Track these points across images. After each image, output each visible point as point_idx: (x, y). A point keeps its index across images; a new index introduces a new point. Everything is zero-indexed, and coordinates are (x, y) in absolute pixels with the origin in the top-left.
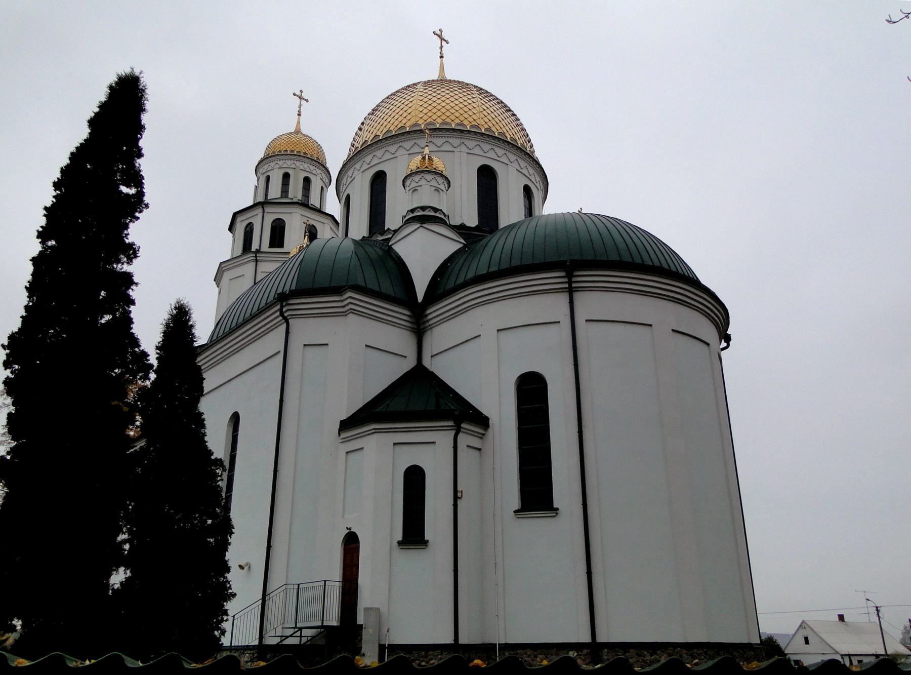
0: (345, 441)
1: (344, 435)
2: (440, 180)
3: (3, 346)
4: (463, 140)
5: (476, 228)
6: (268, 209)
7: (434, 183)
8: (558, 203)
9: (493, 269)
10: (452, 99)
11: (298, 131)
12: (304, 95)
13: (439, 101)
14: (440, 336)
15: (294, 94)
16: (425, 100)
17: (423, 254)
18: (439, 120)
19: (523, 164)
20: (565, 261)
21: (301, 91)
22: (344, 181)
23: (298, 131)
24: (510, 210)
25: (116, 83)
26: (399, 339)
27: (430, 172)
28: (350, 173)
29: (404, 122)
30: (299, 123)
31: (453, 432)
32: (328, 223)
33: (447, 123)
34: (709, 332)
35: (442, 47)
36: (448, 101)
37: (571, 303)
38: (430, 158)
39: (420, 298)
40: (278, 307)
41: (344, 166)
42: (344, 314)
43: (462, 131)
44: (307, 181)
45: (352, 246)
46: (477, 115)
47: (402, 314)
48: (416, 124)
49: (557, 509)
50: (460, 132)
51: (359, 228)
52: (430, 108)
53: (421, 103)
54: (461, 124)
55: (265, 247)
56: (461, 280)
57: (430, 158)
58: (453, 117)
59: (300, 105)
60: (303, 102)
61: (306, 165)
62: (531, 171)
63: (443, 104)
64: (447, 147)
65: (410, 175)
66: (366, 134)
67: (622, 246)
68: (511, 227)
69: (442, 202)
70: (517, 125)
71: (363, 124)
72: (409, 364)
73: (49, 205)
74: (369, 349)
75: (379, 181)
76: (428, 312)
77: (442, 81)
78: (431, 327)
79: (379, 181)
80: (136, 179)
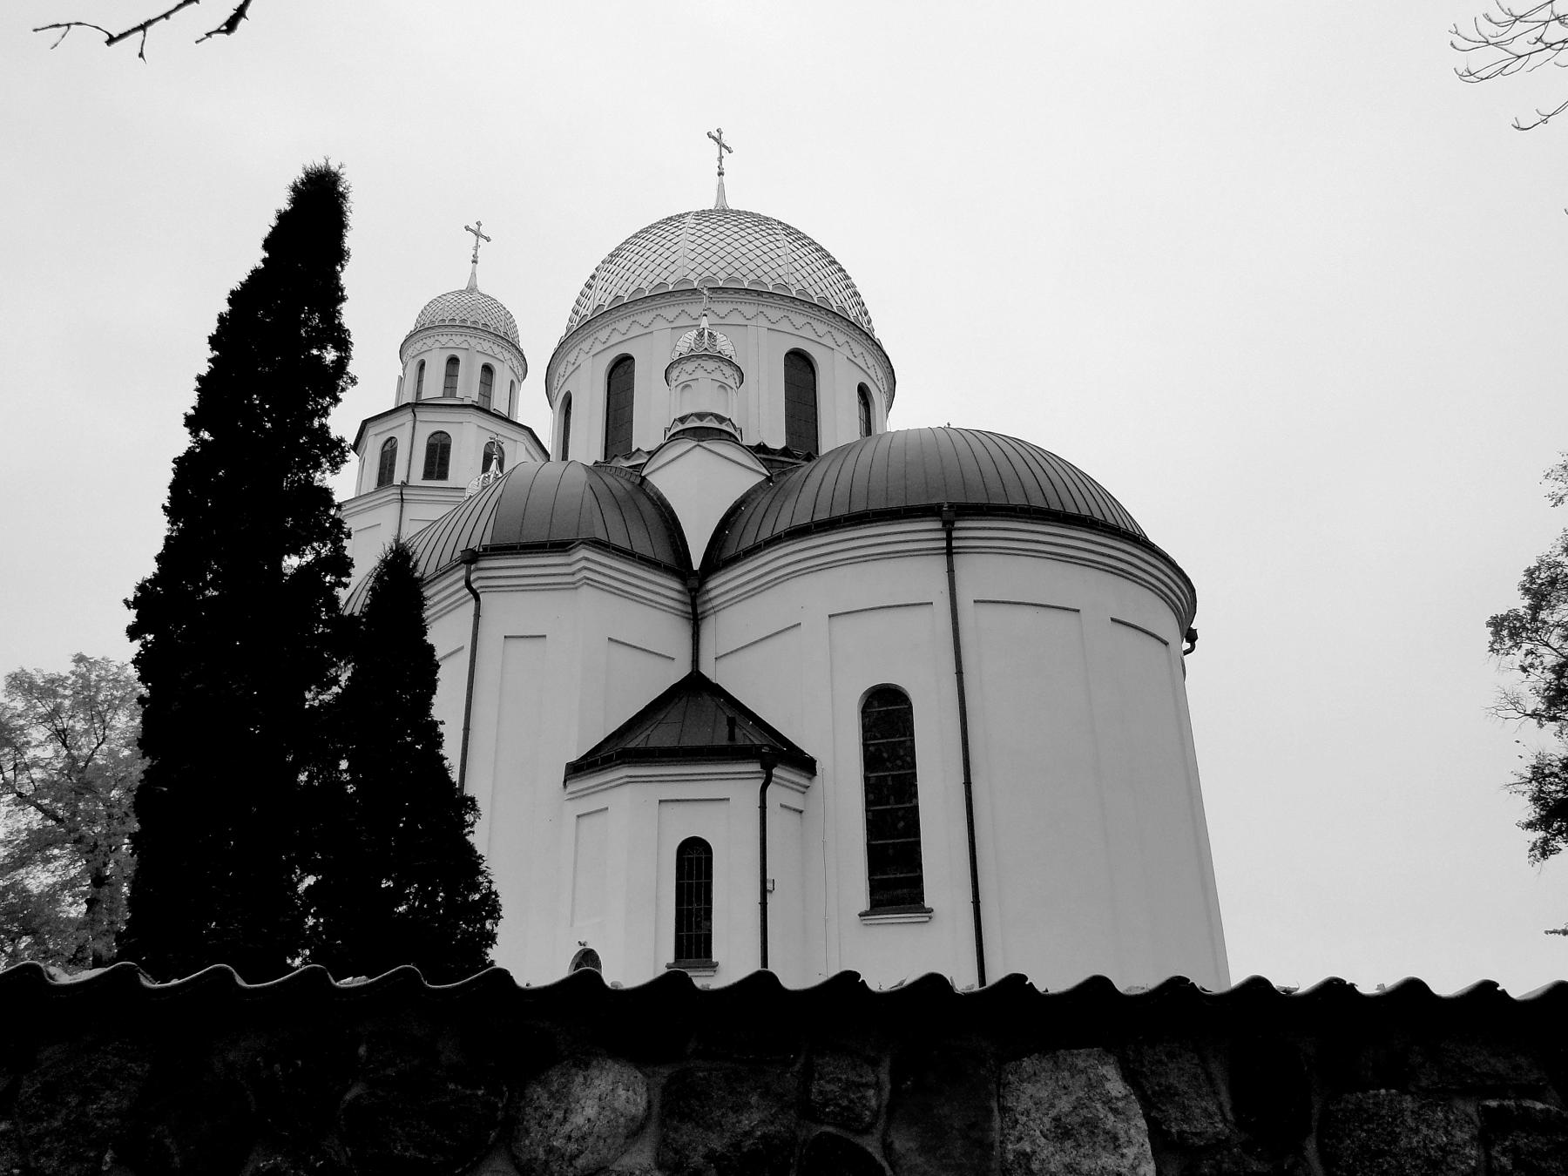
0: (574, 797)
1: (573, 787)
2: (728, 371)
3: (126, 602)
4: (761, 309)
5: (785, 451)
6: (423, 415)
7: (717, 375)
8: (911, 412)
9: (822, 515)
10: (744, 242)
11: (472, 289)
12: (483, 231)
13: (722, 244)
14: (724, 630)
15: (467, 228)
16: (700, 241)
17: (701, 491)
18: (723, 275)
19: (858, 349)
20: (940, 506)
21: (479, 224)
22: (561, 370)
23: (472, 289)
24: (837, 424)
25: (303, 183)
26: (668, 633)
27: (711, 357)
28: (571, 358)
29: (664, 275)
30: (474, 274)
31: (761, 782)
32: (523, 438)
33: (736, 280)
34: (1167, 625)
35: (721, 158)
36: (736, 244)
37: (951, 570)
38: (710, 334)
39: (696, 565)
40: (463, 573)
41: (561, 345)
42: (574, 586)
43: (760, 293)
44: (487, 370)
45: (583, 476)
46: (784, 269)
47: (669, 587)
48: (685, 280)
49: (930, 911)
50: (757, 294)
51: (588, 444)
52: (707, 254)
53: (693, 246)
54: (759, 282)
55: (417, 477)
56: (765, 534)
57: (710, 334)
58: (744, 271)
59: (477, 247)
60: (482, 241)
61: (486, 345)
62: (871, 362)
63: (729, 249)
64: (736, 319)
65: (679, 361)
66: (599, 294)
67: (1029, 482)
68: (845, 450)
69: (730, 407)
70: (847, 286)
71: (593, 277)
72: (678, 671)
73: (204, 371)
74: (614, 645)
75: (622, 368)
76: (710, 585)
77: (722, 214)
78: (716, 611)
79: (622, 368)
80: (342, 342)
